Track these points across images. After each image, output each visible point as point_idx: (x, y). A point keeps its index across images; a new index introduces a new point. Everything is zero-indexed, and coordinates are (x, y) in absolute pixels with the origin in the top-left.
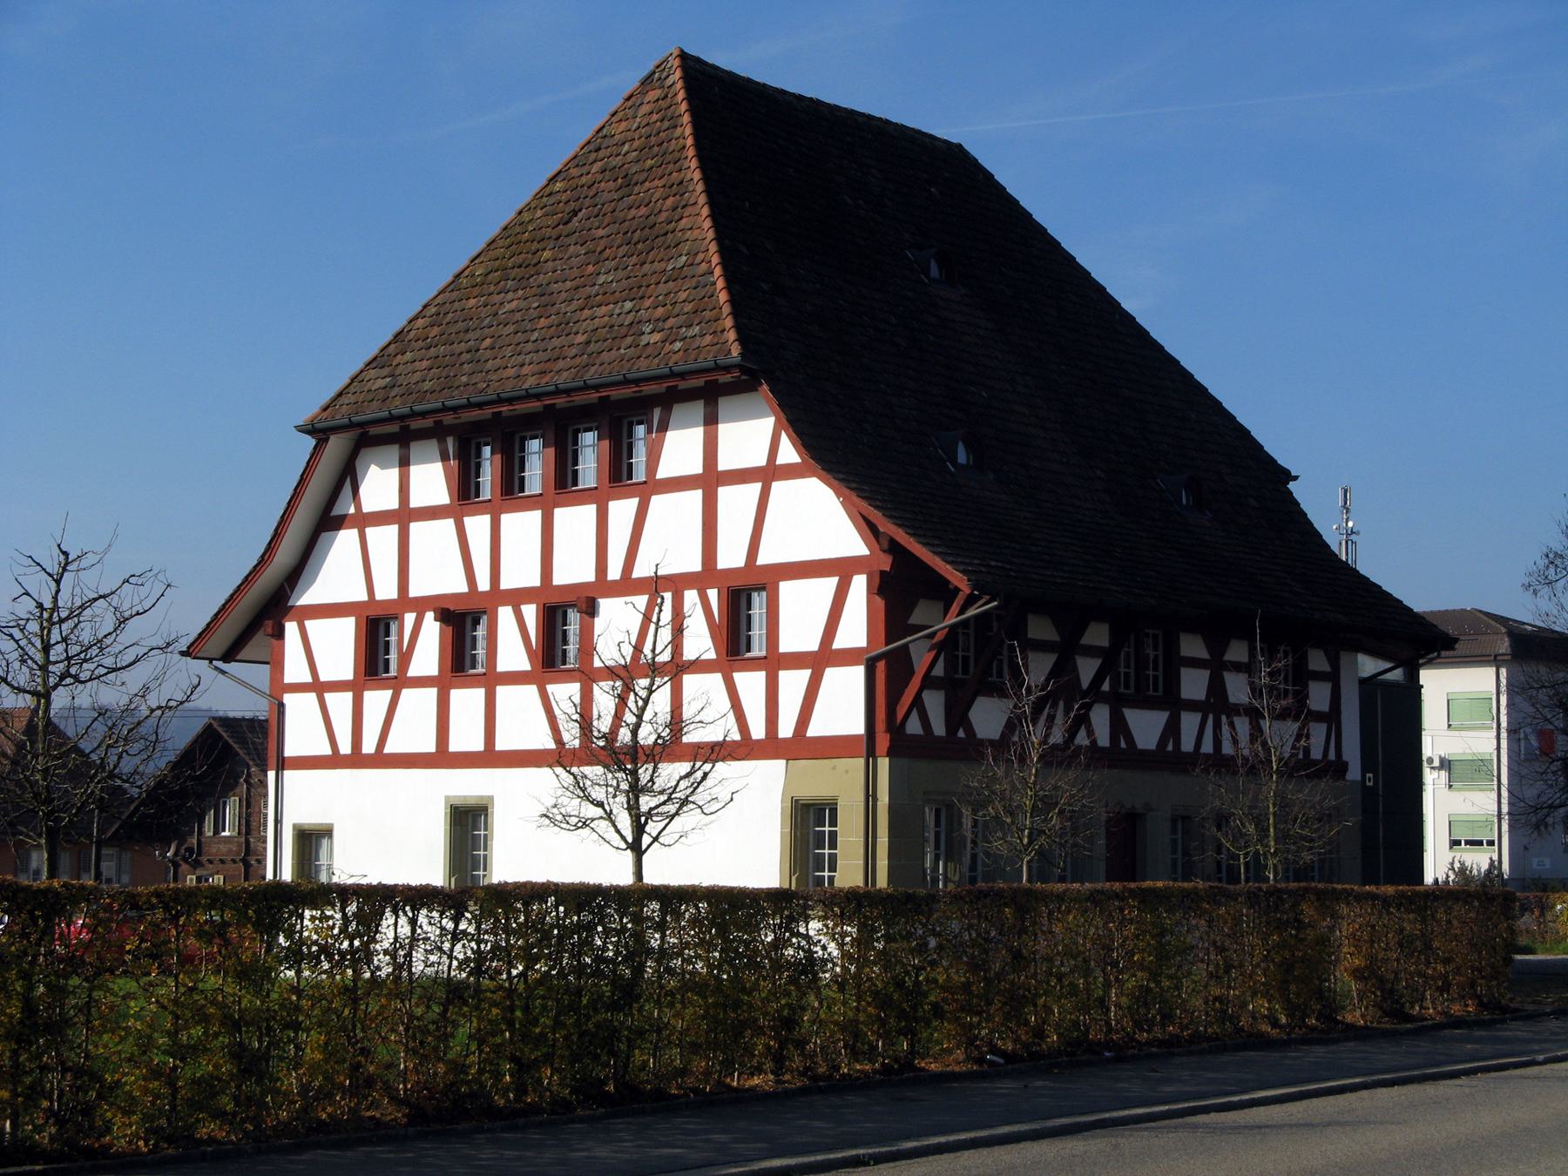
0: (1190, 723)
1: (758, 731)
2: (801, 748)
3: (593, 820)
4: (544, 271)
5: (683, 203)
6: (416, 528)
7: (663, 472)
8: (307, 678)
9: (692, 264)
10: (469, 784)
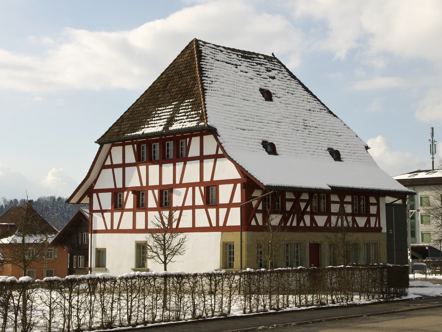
0: (334, 219)
1: (214, 224)
2: (225, 229)
3: (155, 256)
4: (159, 100)
5: (195, 83)
6: (127, 169)
7: (189, 156)
8: (99, 209)
9: (197, 100)
10: (142, 237)
